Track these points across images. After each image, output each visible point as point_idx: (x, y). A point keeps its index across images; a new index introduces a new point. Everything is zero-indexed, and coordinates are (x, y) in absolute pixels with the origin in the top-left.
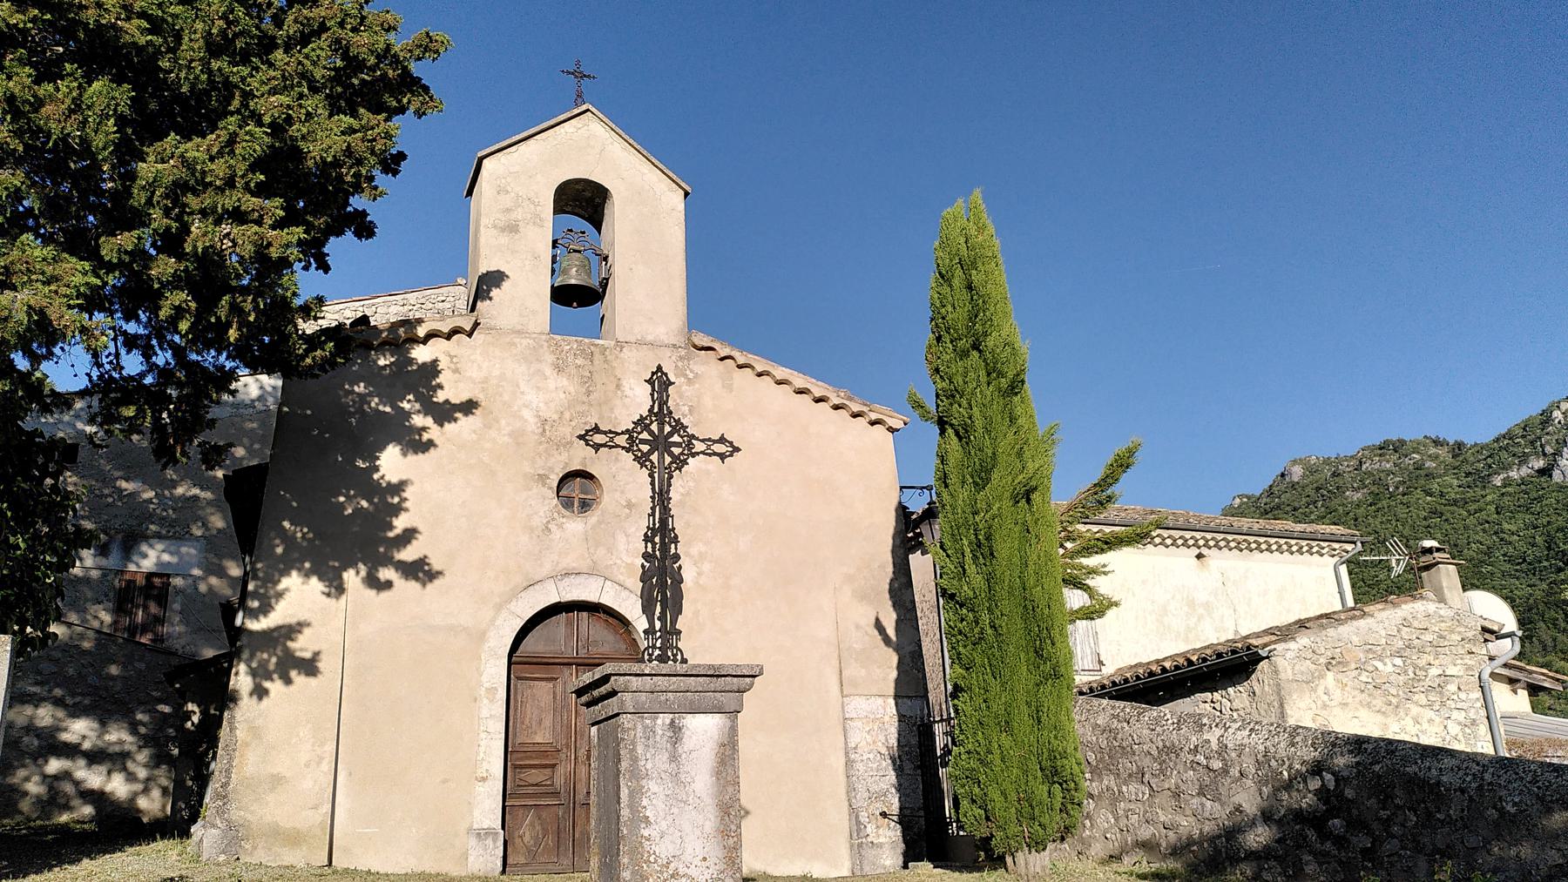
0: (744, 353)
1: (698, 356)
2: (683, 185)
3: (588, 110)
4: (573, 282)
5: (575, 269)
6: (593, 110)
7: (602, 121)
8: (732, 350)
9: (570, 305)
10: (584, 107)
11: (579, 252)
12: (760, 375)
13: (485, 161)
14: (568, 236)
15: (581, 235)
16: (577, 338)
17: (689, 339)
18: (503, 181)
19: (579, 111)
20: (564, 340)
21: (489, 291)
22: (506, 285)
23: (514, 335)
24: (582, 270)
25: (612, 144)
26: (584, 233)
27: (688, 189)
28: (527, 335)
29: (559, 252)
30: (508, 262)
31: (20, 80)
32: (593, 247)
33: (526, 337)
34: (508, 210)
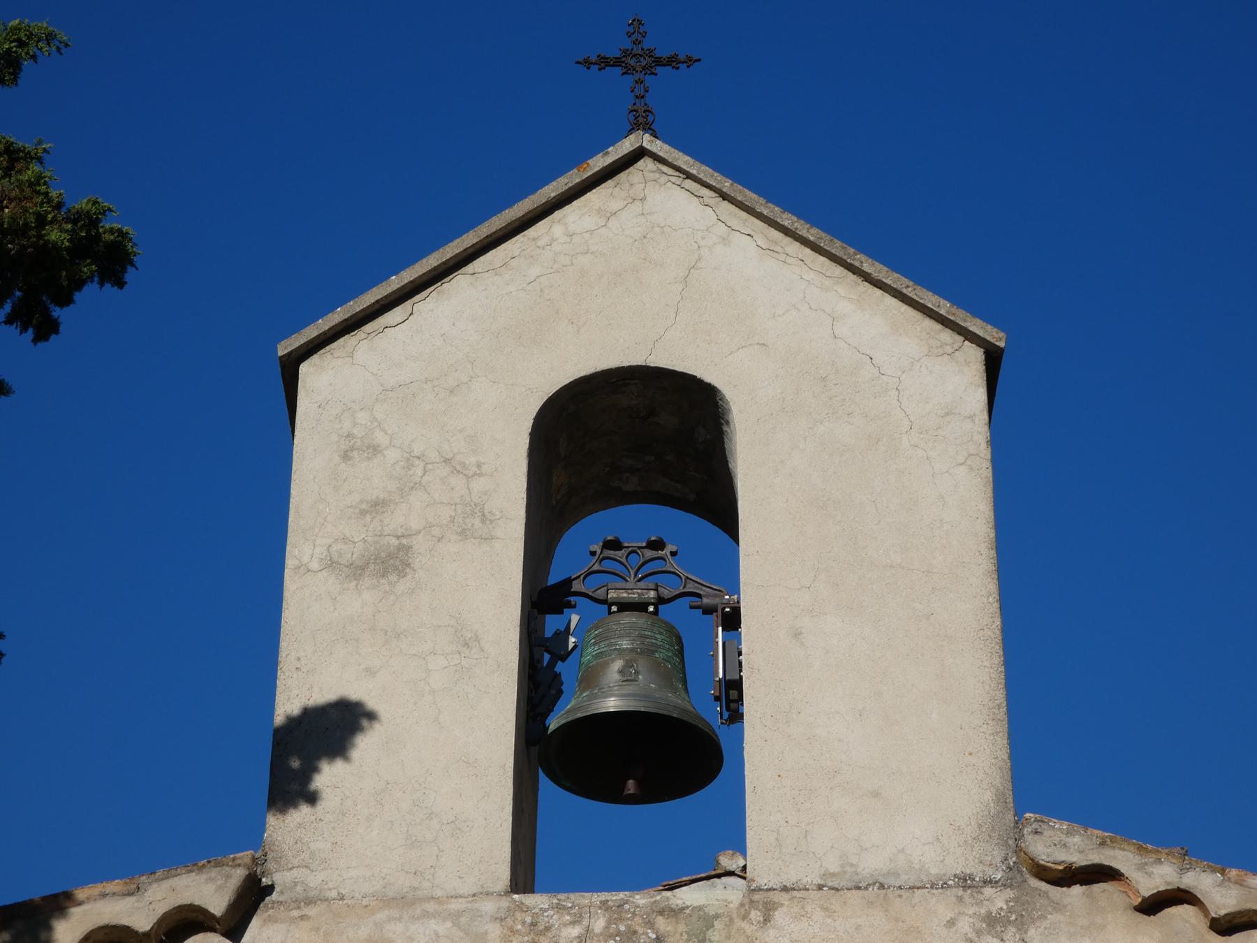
0: (1233, 873)
1: (1058, 907)
2: (976, 326)
3: (639, 154)
4: (612, 704)
5: (618, 664)
6: (656, 146)
7: (689, 176)
8: (1182, 871)
9: (614, 795)
10: (627, 145)
11: (640, 607)
12: (1153, 906)
13: (304, 368)
14: (607, 565)
15: (649, 554)
16: (604, 896)
17: (1019, 851)
18: (363, 417)
19: (609, 160)
20: (559, 908)
21: (310, 770)
22: (365, 745)
23: (381, 916)
24: (642, 664)
25: (725, 241)
26: (657, 545)
27: (997, 337)
28: (431, 907)
29: (575, 619)
30: (370, 672)
31: (594, 941)
32: (691, 588)
33: (426, 915)
34: (378, 506)
